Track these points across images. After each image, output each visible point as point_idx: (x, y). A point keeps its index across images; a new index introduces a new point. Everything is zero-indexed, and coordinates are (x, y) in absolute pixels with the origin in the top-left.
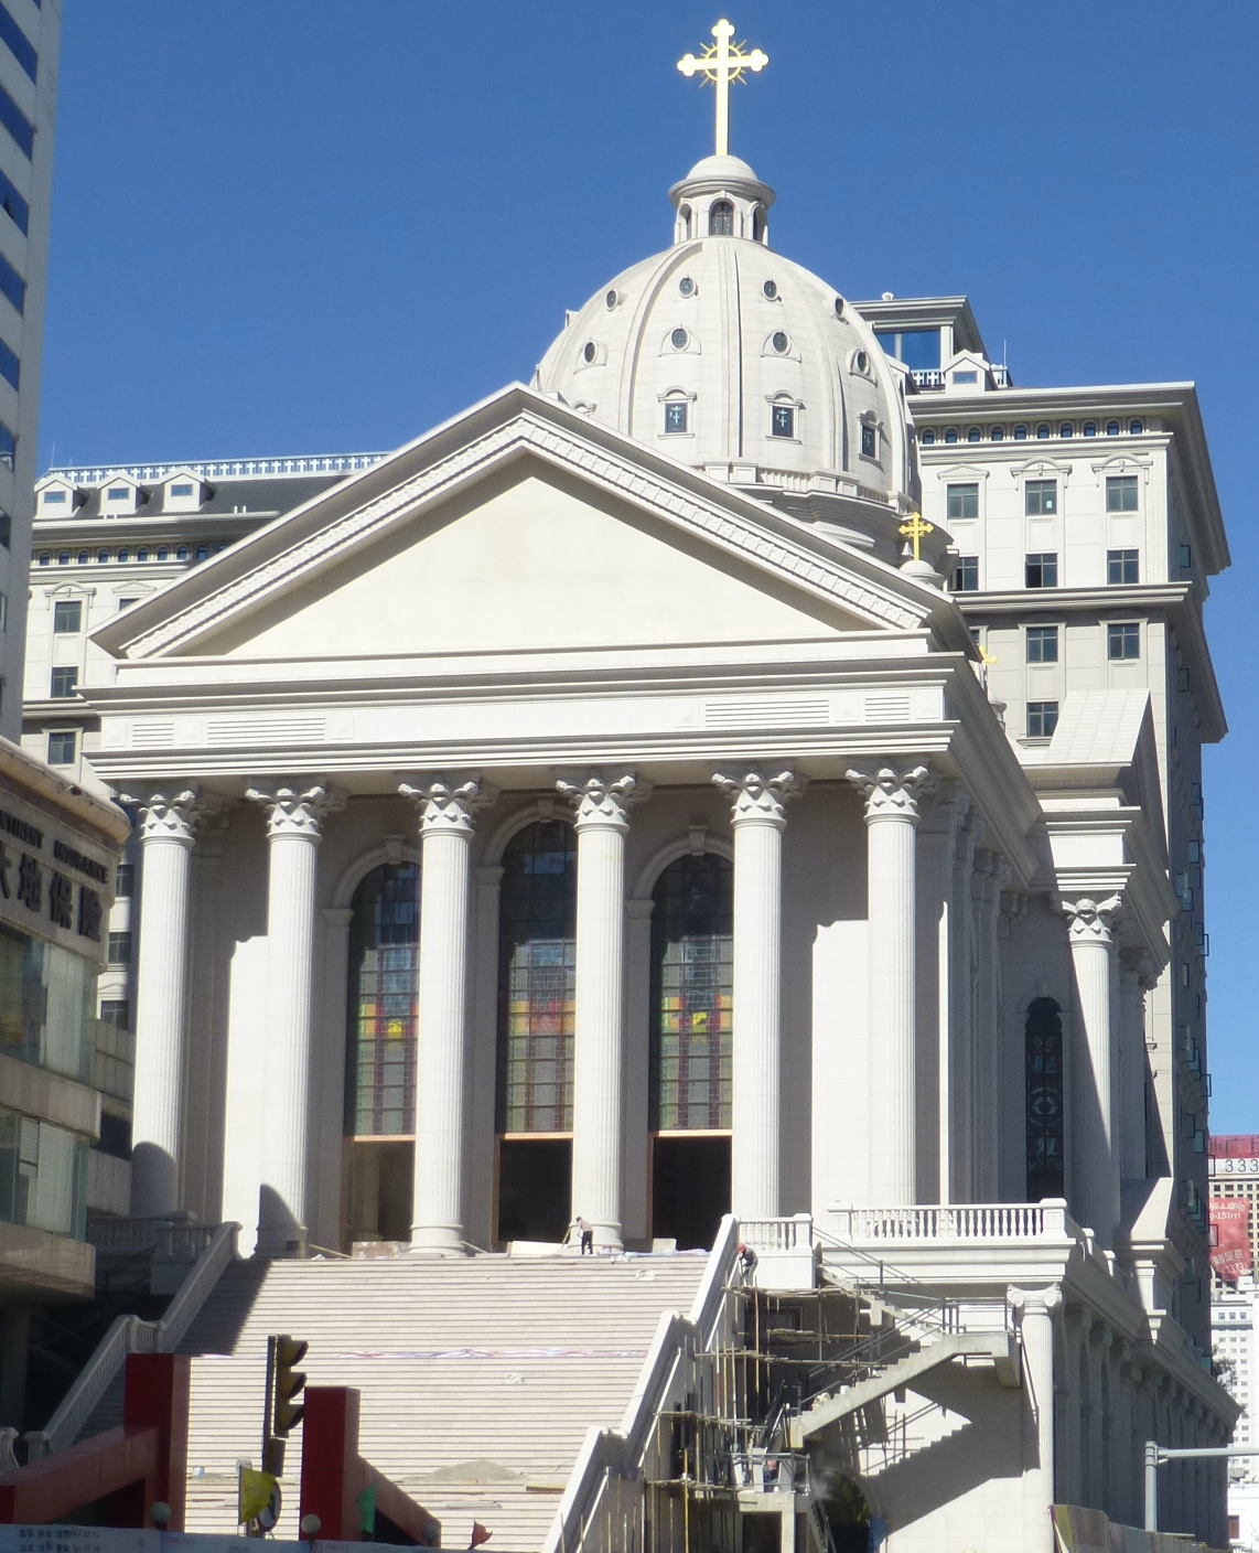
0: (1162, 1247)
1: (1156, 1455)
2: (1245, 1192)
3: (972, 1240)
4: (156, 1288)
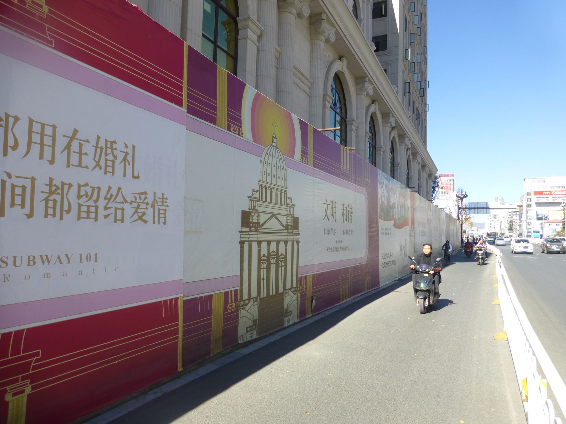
0: (239, 308)
1: (40, 350)
2: (450, 181)
3: (36, 13)
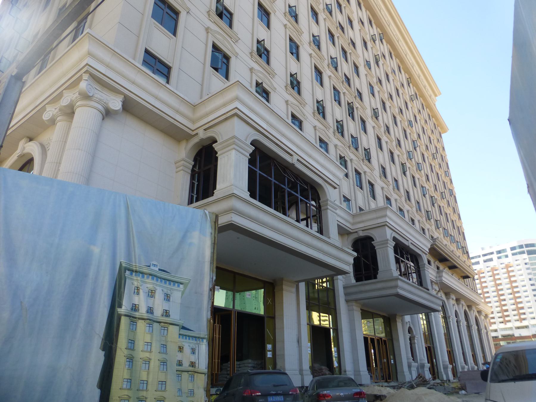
4: (291, 77)
